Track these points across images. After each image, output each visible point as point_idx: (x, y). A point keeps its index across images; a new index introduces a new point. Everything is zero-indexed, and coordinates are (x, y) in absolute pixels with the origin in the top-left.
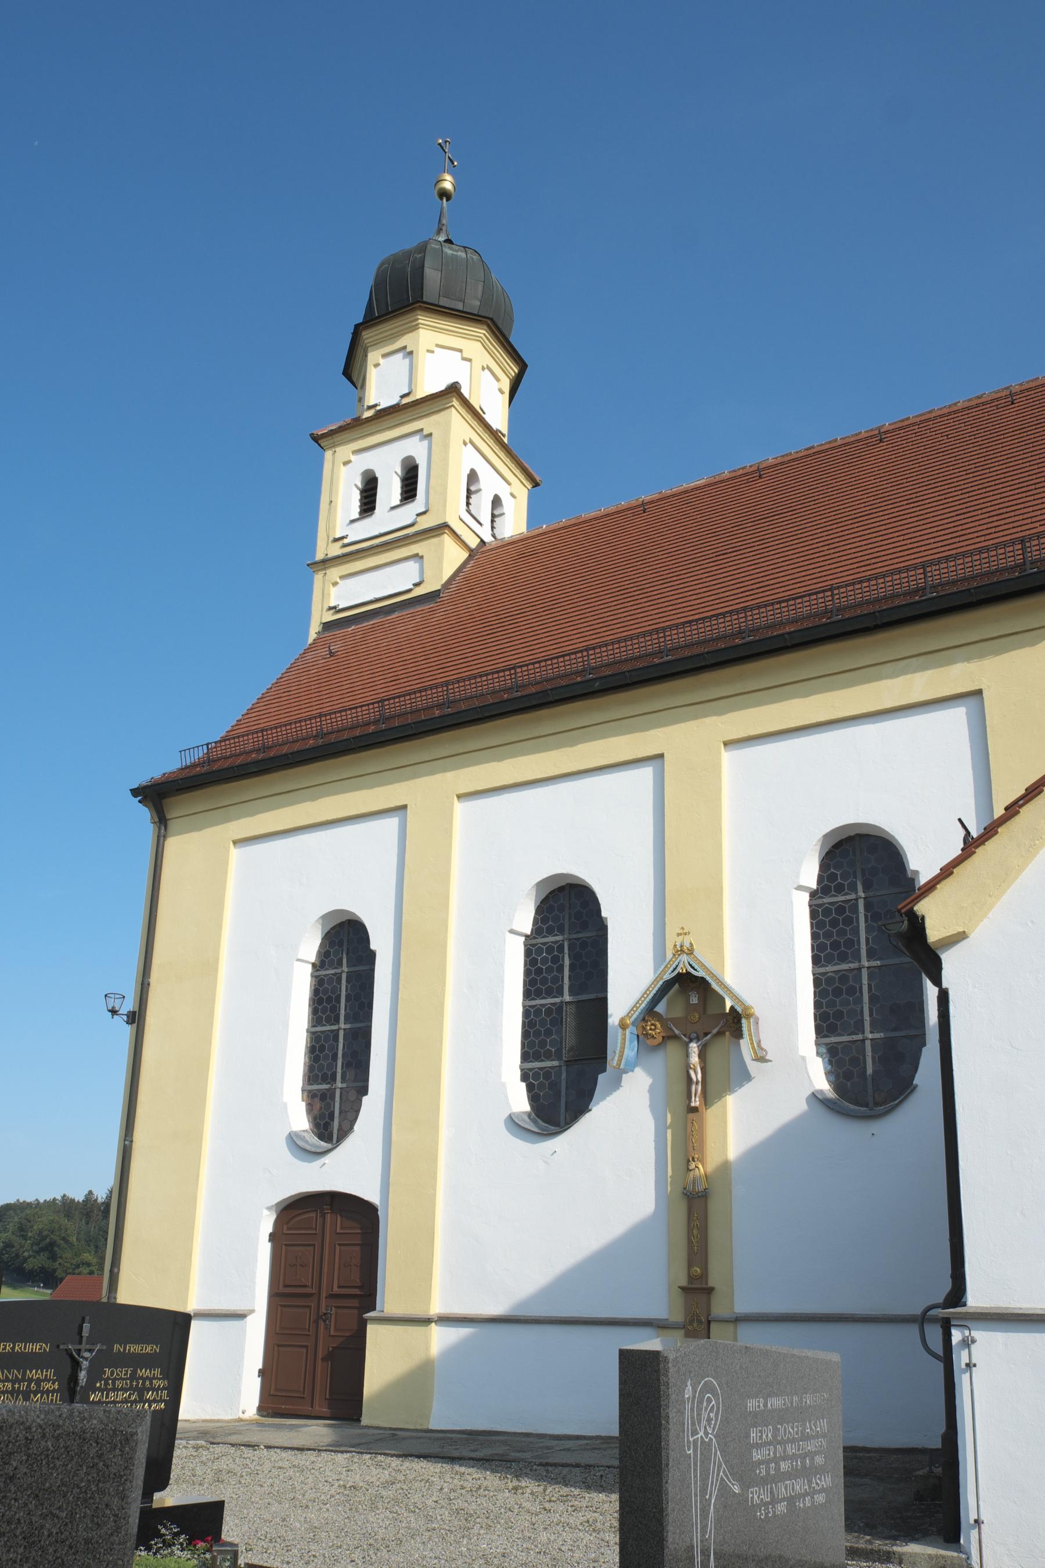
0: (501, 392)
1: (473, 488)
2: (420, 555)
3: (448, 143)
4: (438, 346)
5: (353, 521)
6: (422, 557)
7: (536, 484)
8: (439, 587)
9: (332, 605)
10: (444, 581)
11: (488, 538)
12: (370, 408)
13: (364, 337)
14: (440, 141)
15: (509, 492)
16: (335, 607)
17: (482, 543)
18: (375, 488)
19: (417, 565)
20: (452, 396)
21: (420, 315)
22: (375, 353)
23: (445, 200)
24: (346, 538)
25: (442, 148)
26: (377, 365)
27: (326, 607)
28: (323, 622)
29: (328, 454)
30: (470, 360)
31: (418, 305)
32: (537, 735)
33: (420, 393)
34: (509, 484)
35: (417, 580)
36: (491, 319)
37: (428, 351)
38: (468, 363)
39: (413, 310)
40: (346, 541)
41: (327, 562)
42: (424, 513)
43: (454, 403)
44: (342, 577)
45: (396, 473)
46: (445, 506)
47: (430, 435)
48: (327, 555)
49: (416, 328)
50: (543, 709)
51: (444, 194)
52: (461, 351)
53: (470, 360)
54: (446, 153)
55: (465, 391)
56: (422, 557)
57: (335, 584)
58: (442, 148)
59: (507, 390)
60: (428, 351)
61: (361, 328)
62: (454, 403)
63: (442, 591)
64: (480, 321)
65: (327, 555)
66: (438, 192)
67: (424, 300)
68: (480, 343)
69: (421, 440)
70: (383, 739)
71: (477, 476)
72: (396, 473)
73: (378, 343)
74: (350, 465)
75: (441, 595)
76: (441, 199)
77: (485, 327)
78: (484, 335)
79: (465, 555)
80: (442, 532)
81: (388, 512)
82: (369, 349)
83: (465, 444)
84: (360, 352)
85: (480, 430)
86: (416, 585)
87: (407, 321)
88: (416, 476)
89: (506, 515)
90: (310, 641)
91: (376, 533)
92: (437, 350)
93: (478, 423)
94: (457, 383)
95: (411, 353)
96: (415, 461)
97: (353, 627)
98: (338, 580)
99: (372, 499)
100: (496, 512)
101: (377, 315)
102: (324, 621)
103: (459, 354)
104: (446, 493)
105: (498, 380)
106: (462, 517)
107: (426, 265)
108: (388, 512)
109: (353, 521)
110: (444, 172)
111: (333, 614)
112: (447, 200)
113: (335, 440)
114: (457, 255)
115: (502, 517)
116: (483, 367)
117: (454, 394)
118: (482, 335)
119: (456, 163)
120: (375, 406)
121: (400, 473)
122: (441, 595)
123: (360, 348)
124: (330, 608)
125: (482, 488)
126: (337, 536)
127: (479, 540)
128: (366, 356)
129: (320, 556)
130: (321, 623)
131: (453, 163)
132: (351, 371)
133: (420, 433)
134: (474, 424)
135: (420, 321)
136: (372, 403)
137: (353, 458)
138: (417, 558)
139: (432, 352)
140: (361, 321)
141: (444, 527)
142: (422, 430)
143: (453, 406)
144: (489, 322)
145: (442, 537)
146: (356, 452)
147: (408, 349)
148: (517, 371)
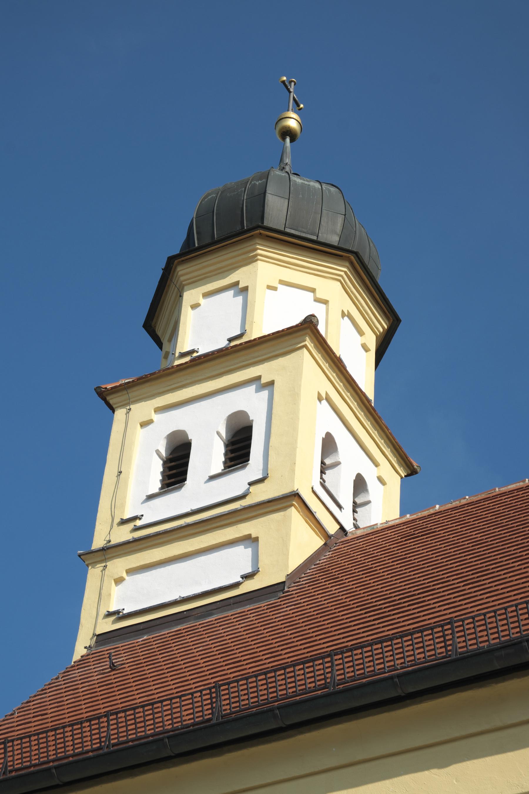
0: (366, 348)
1: (328, 461)
2: (253, 536)
3: (293, 84)
4: (282, 282)
5: (151, 497)
6: (256, 540)
7: (412, 472)
8: (283, 579)
9: (112, 609)
10: (290, 571)
11: (349, 526)
12: (183, 355)
13: (180, 273)
14: (285, 78)
15: (377, 475)
16: (117, 612)
17: (342, 533)
18: (187, 456)
19: (249, 551)
20: (305, 334)
21: (259, 244)
22: (193, 291)
23: (288, 140)
24: (140, 519)
25: (286, 87)
26: (194, 306)
27: (103, 611)
28: (97, 633)
29: (120, 414)
30: (325, 302)
31: (258, 231)
32: (499, 724)
33: (255, 333)
34: (376, 464)
35: (249, 570)
36: (356, 254)
37: (269, 287)
38: (323, 306)
39: (252, 237)
40: (139, 523)
41: (109, 551)
42: (260, 481)
43: (306, 343)
44: (131, 572)
45: (218, 433)
46: (293, 471)
47: (271, 383)
48: (110, 541)
49: (253, 260)
50: (512, 678)
51: (288, 133)
52: (313, 290)
53: (325, 302)
54: (290, 92)
55: (321, 328)
56: (256, 540)
57: (119, 581)
58: (286, 87)
59: (373, 346)
60: (269, 287)
61: (176, 261)
62: (306, 343)
63: (287, 585)
64: (341, 256)
65: (110, 541)
66: (280, 131)
67: (266, 224)
68: (339, 283)
69: (257, 391)
70: (222, 739)
71: (335, 443)
72: (218, 433)
73: (195, 282)
74: (151, 426)
75: (286, 589)
76: (284, 139)
77: (347, 264)
78: (345, 272)
79: (318, 542)
80: (288, 504)
81: (206, 482)
82: (186, 288)
83: (320, 399)
84: (171, 292)
85: (340, 386)
86: (247, 577)
87: (240, 252)
88: (249, 438)
89: (372, 504)
90: (77, 657)
91: (187, 510)
92: (280, 287)
93: (337, 375)
94: (313, 316)
95: (245, 289)
96: (248, 417)
97: (145, 637)
98: (124, 575)
99: (183, 469)
100: (359, 501)
101: (197, 245)
102: (99, 631)
103: (312, 294)
104: (295, 455)
105: (361, 333)
106: (315, 489)
107: (268, 191)
108: (206, 482)
109: (151, 497)
110: (288, 111)
111: (114, 622)
112: (292, 141)
113: (130, 395)
114: (309, 185)
115: (367, 507)
116: (343, 311)
117: (308, 331)
118: (342, 273)
119: (302, 106)
120: (193, 351)
121: (224, 434)
122: (286, 589)
123: (172, 287)
124: (110, 614)
125: (341, 460)
126: (126, 516)
127: (338, 527)
128: (181, 296)
129: (98, 543)
130: (94, 635)
131: (299, 106)
132: (156, 323)
133: (257, 382)
134: (333, 376)
135: (259, 252)
136: (186, 349)
137: (155, 417)
138: (247, 542)
139: (275, 289)
140: (177, 251)
141: (296, 495)
142: (259, 378)
143: (305, 346)
144: (352, 258)
145: (289, 510)
146: (159, 410)
147: (241, 285)
148: (386, 327)
